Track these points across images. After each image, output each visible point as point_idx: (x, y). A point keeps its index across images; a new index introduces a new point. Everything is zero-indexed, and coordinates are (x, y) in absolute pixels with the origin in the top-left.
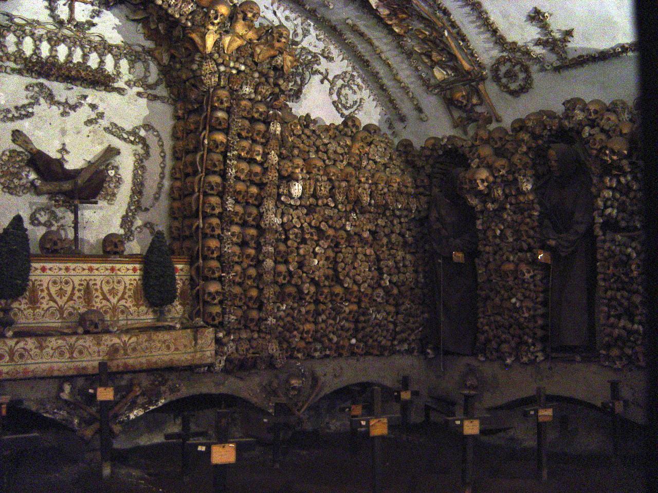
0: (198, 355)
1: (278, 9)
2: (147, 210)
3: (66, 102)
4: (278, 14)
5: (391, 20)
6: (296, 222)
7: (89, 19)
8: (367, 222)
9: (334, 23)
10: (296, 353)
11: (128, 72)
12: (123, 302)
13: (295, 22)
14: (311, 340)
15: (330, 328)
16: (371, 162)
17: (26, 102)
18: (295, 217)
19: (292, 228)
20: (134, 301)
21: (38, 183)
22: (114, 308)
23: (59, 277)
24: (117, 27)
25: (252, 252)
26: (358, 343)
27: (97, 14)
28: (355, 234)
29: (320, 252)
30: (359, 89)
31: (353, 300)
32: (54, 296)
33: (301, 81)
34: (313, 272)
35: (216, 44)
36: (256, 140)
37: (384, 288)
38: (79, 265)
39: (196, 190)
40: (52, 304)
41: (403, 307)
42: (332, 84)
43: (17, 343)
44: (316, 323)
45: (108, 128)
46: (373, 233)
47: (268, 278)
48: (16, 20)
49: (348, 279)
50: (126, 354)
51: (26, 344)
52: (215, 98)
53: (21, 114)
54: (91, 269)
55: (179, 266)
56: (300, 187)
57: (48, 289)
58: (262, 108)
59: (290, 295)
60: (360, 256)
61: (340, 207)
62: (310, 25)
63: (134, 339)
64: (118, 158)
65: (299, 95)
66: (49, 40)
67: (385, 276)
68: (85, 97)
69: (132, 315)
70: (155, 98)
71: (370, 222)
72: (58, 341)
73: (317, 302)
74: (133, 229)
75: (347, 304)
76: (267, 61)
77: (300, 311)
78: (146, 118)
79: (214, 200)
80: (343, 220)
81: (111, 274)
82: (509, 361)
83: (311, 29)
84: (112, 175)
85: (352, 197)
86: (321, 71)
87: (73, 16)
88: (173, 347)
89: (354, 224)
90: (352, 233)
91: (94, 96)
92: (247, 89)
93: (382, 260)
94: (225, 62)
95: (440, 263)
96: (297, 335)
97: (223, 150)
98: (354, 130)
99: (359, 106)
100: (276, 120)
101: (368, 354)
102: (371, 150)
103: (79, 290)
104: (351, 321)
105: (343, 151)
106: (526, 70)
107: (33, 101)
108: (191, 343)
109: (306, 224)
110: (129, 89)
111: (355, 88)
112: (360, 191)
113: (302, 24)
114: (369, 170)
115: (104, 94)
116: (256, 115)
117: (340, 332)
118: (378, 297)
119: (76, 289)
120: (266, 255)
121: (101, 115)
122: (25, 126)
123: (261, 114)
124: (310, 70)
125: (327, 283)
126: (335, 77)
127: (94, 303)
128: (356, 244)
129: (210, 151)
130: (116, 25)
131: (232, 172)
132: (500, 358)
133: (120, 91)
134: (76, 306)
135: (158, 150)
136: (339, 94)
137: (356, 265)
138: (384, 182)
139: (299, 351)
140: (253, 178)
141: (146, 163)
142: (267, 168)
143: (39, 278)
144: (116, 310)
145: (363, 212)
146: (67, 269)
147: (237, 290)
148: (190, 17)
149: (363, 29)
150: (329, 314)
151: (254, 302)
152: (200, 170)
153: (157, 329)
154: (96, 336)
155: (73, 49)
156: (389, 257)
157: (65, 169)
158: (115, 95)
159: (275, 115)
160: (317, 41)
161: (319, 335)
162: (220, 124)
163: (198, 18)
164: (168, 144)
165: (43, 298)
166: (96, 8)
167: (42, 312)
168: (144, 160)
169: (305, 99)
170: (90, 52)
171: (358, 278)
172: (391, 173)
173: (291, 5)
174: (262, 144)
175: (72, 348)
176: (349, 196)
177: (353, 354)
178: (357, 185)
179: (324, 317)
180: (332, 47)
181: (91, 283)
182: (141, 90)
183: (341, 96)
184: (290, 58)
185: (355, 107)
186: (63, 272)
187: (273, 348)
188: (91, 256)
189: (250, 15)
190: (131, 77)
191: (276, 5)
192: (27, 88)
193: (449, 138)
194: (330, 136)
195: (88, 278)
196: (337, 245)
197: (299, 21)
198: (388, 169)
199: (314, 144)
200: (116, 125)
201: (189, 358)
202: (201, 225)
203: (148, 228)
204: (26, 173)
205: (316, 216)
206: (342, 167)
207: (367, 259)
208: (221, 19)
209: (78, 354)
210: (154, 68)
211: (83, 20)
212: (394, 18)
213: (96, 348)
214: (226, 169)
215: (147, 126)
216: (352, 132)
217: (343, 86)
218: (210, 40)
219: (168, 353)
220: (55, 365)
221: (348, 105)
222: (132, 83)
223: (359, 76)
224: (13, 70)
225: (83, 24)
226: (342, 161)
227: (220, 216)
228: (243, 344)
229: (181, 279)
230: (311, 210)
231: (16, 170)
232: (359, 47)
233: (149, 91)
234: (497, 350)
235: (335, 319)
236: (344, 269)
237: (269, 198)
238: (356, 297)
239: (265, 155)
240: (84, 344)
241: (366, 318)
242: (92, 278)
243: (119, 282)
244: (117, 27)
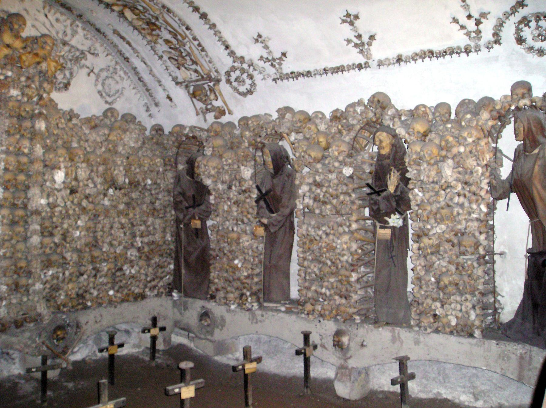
4: (49, 16)
6: (60, 202)
41: (153, 262)
42: (98, 76)
62: (78, 26)
75: (105, 264)
82: (233, 307)
95: (181, 228)
106: (251, 77)
109: (69, 203)
111: (118, 79)
116: (23, 114)
132: (226, 304)
136: (103, 84)
180: (98, 45)
183: (106, 87)
185: (117, 95)
191: (46, 11)
193: (192, 128)
197: (69, 22)
217: (107, 77)
221: (111, 94)
226: (101, 148)
234: (225, 298)
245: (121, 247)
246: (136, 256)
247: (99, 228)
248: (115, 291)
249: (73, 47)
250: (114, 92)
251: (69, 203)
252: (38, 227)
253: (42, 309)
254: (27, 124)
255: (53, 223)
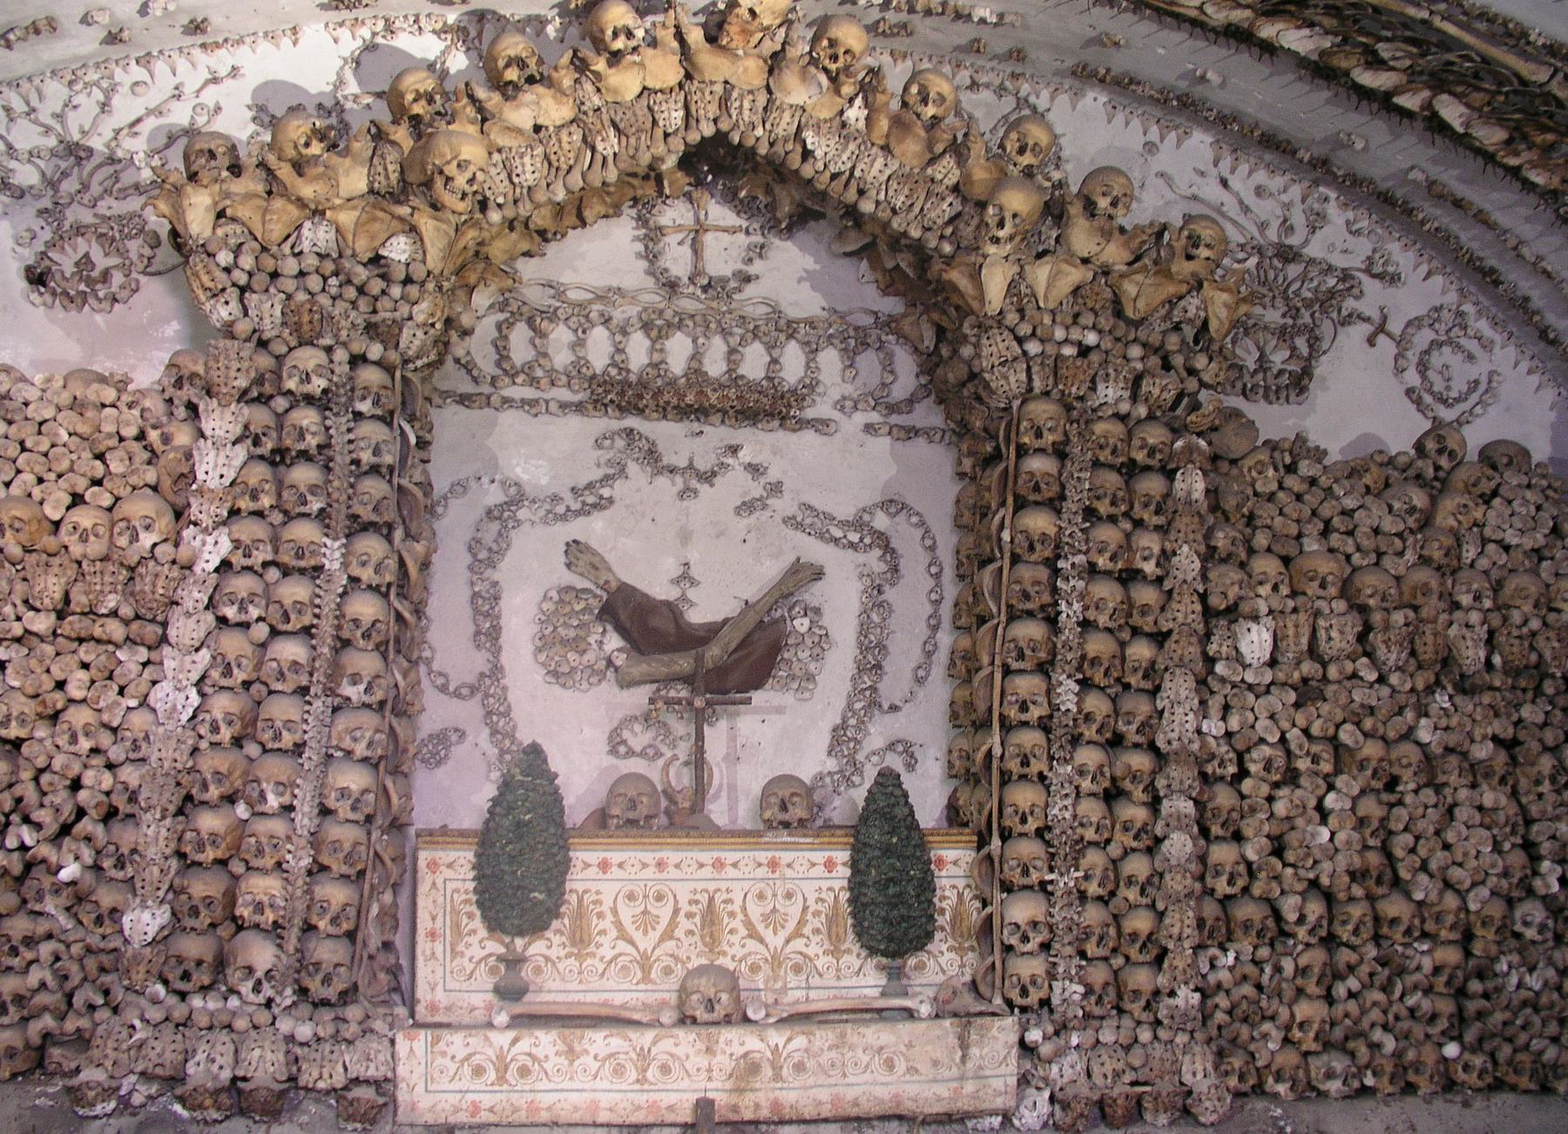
0: (969, 1087)
1: (1233, 171)
2: (894, 708)
3: (691, 466)
4: (1235, 183)
5: (1517, 154)
7: (740, 266)
8: (1485, 717)
9: (1383, 186)
10: (1270, 1080)
11: (839, 380)
12: (798, 944)
13: (1285, 198)
14: (1314, 1047)
15: (1375, 1015)
16: (1491, 547)
17: (597, 474)
18: (1263, 715)
19: (1256, 745)
20: (826, 942)
21: (620, 659)
22: (776, 961)
23: (642, 884)
24: (810, 277)
25: (1137, 814)
26: (1467, 1056)
27: (761, 251)
28: (1449, 750)
29: (1338, 807)
30: (1484, 347)
31: (1444, 934)
32: (630, 928)
33: (1311, 346)
34: (1316, 862)
35: (1012, 288)
36: (1142, 520)
37: (1547, 900)
38: (690, 854)
39: (985, 660)
40: (623, 946)
42: (1402, 342)
43: (515, 1041)
44: (1329, 999)
45: (794, 517)
46: (1508, 745)
47: (1177, 883)
48: (572, 295)
49: (1423, 878)
50: (777, 1077)
51: (676, 1045)
52: (1024, 424)
53: (584, 503)
54: (719, 865)
55: (949, 854)
56: (1267, 637)
57: (615, 911)
58: (1155, 435)
59: (1247, 925)
60: (1462, 813)
61: (1394, 679)
63: (800, 1042)
64: (817, 587)
65: (1305, 382)
66: (646, 327)
67: (1546, 865)
68: (734, 450)
69: (821, 975)
70: (911, 432)
71: (1496, 715)
72: (610, 1040)
73: (1330, 941)
74: (860, 757)
75: (1425, 947)
76: (1163, 312)
77: (1278, 969)
78: (887, 485)
79: (1027, 685)
80: (1409, 715)
81: (770, 875)
83: (1332, 209)
84: (803, 629)
85: (1427, 652)
86: (1367, 313)
87: (700, 265)
88: (901, 1066)
89: (1443, 723)
90: (1437, 750)
91: (757, 443)
92: (1110, 392)
93: (1534, 821)
94: (1039, 331)
96: (1274, 1033)
97: (1048, 553)
98: (1444, 462)
99: (1487, 391)
100: (1193, 462)
101: (1498, 1086)
102: (1491, 514)
103: (689, 916)
104: (1441, 994)
105: (1402, 527)
107: (612, 471)
108: (952, 1052)
110: (844, 418)
111: (1472, 346)
112: (1453, 631)
113: (1303, 201)
114: (1486, 573)
115: (781, 437)
116: (1140, 456)
117: (1405, 1025)
118: (1526, 924)
119: (682, 913)
120: (1173, 823)
121: (776, 488)
122: (594, 529)
123: (1152, 452)
124: (1334, 315)
125: (1358, 891)
126: (1409, 324)
127: (726, 948)
128: (1453, 779)
129: (1015, 559)
130: (806, 271)
131: (1070, 612)
133: (821, 426)
134: (682, 954)
135: (925, 559)
136: (1423, 367)
137: (1450, 836)
138: (1531, 601)
139: (1278, 1078)
140: (1136, 620)
141: (890, 594)
142: (1170, 592)
143: (593, 886)
144: (780, 964)
145: (1465, 687)
146: (719, 865)
147: (1093, 915)
148: (949, 231)
149: (1461, 190)
150: (1371, 975)
151: (1144, 945)
152: (994, 610)
153: (881, 1014)
154: (703, 1031)
155: (701, 341)
156: (1558, 811)
157: (690, 624)
158: (809, 436)
159: (1190, 449)
160: (1349, 237)
161: (1338, 1033)
162: (1037, 489)
163: (967, 231)
164: (947, 541)
165: (603, 932)
166: (758, 239)
167: (601, 967)
168: (886, 588)
169: (1326, 389)
170: (743, 342)
171: (1456, 873)
172: (1557, 575)
173: (1268, 157)
174: (1157, 528)
175: (644, 1056)
176: (1420, 649)
177: (1450, 1086)
178: (1444, 617)
179: (1353, 983)
180: (1394, 247)
181: (719, 898)
182: (875, 417)
183: (1430, 373)
184: (1225, 296)
185: (1474, 397)
186: (650, 872)
187: (1197, 1070)
188: (733, 834)
189: (1103, 203)
190: (849, 389)
191: (1226, 164)
192: (598, 444)
194: (1368, 488)
195: (712, 886)
196: (1392, 783)
197: (1296, 191)
198: (1545, 564)
199: (1314, 513)
200: (810, 507)
201: (946, 1094)
202: (997, 751)
203: (900, 754)
204: (598, 637)
205: (1325, 708)
206: (1402, 570)
207: (1487, 820)
208: (1016, 226)
209: (658, 1073)
210: (906, 364)
211: (727, 271)
212: (1523, 146)
213: (703, 1061)
214: (1056, 604)
215: (894, 505)
216: (1437, 468)
217: (1435, 345)
218: (996, 283)
219: (889, 1079)
220: (599, 1096)
221: (1454, 394)
222: (849, 404)
223: (1479, 312)
224: (563, 406)
225: (724, 281)
226: (1401, 554)
227: (1045, 725)
228: (1105, 1057)
229: (954, 887)
230: (1307, 692)
231: (572, 633)
232: (1464, 237)
233: (895, 419)
235: (1386, 988)
236: (1413, 851)
237: (1178, 671)
238: (1452, 927)
239: (1165, 556)
240: (674, 1050)
241: (1490, 985)
242: (723, 885)
243: (789, 896)
244: (810, 277)
245: (1484, 892)
246: (1542, 928)
247: (1398, 819)
248: (1463, 1048)
249: (1312, 261)
250: (1465, 388)
251: (1294, 735)
252: (1188, 807)
253: (1200, 1076)
254: (1152, 485)
255: (1243, 797)
